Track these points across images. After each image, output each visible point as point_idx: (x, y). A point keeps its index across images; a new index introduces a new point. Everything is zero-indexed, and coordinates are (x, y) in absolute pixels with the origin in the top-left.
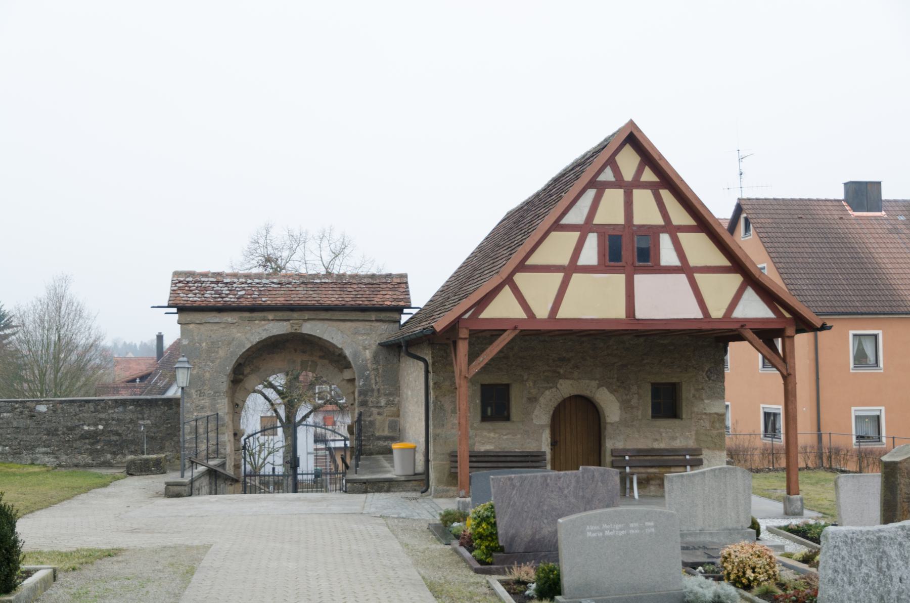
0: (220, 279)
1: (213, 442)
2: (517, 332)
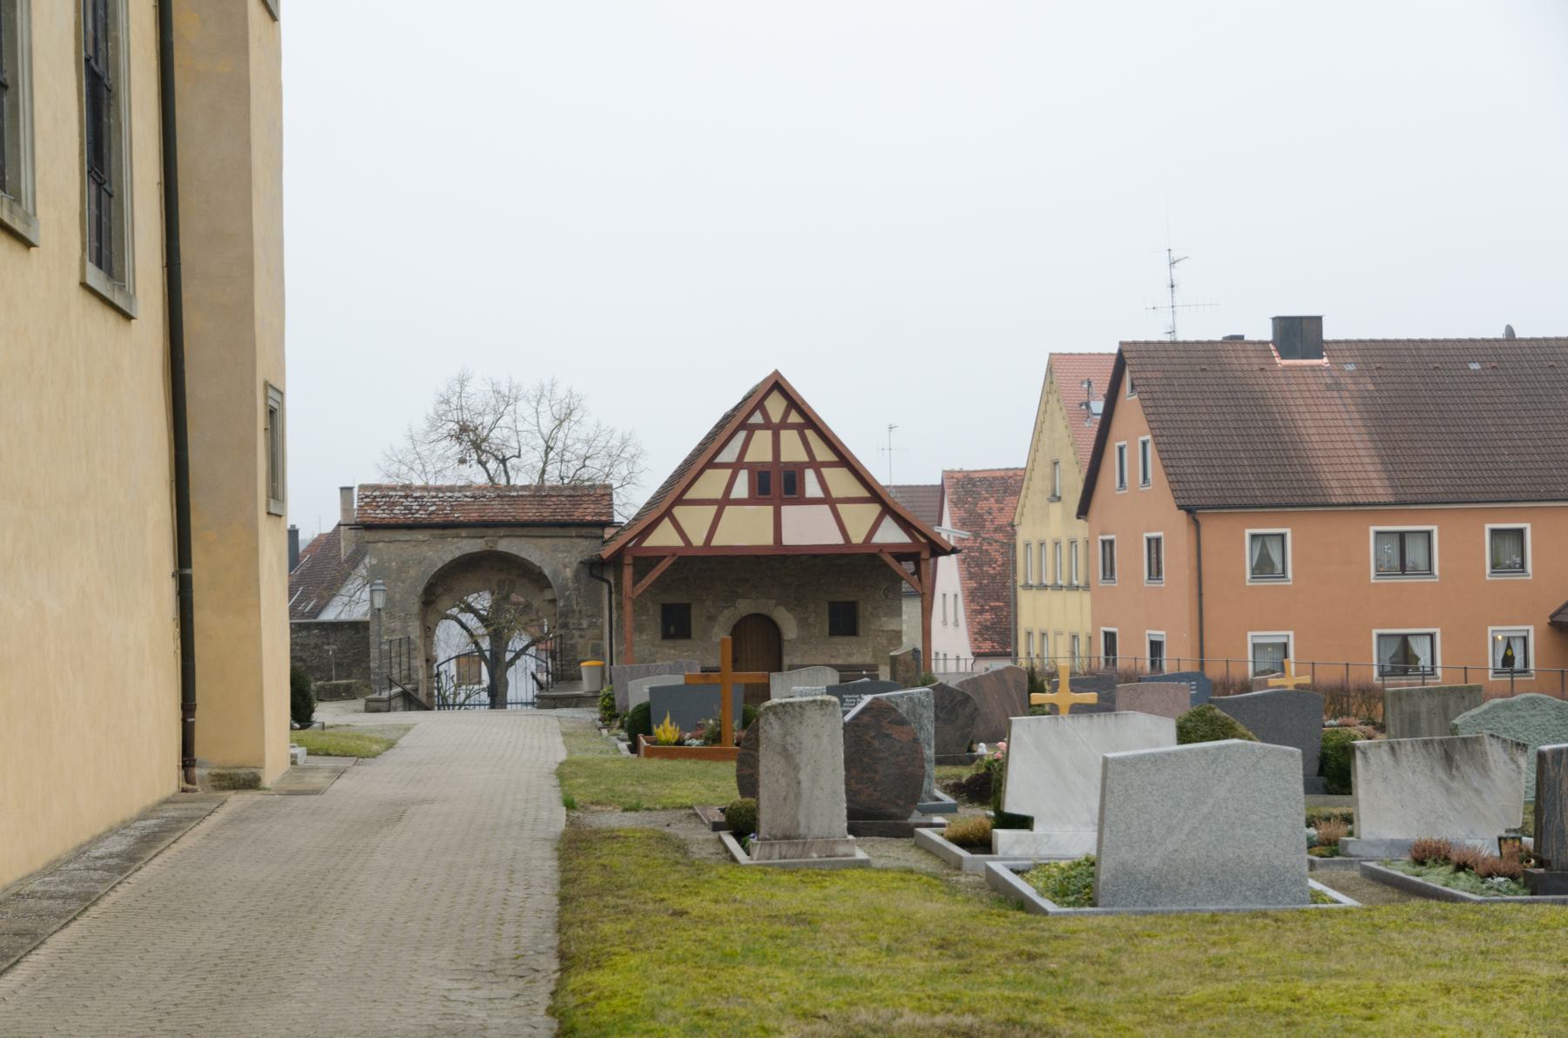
0: (409, 492)
1: (405, 667)
2: (675, 558)
